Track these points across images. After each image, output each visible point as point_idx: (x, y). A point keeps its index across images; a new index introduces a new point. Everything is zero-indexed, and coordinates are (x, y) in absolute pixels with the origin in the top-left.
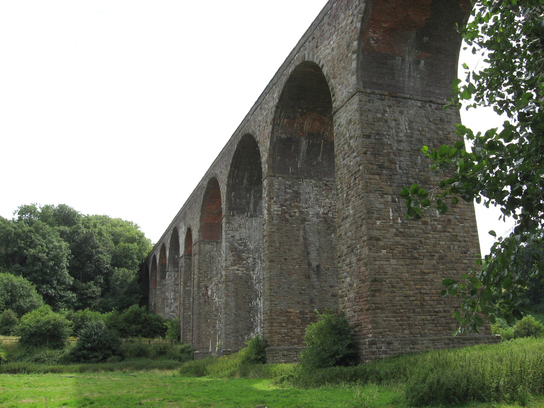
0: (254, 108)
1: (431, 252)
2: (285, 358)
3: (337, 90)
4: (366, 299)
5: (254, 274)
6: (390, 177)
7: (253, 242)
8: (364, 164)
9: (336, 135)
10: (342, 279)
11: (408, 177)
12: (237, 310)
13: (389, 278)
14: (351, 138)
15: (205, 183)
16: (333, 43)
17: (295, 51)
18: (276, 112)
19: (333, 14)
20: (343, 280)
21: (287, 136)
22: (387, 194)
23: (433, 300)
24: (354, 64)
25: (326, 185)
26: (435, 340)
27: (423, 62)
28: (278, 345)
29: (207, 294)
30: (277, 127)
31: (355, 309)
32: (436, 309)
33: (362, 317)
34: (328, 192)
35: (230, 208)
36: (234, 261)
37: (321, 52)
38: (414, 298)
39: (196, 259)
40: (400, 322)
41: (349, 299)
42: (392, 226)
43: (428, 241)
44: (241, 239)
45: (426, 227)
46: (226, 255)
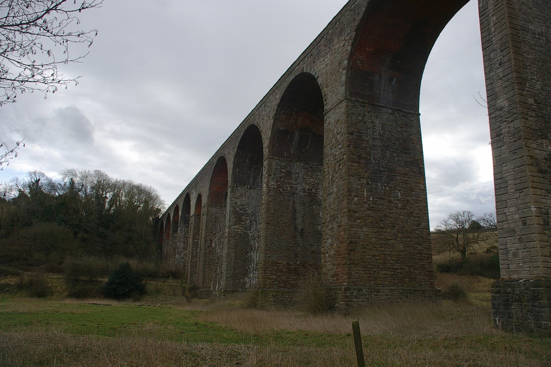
0: (259, 105)
1: (393, 224)
2: (274, 298)
3: (329, 96)
4: (344, 256)
5: (250, 232)
6: (366, 165)
8: (348, 154)
9: (326, 131)
10: (325, 240)
11: (379, 167)
12: (235, 260)
13: (362, 241)
14: (338, 134)
15: (215, 161)
16: (328, 60)
17: (296, 64)
18: (277, 110)
19: (328, 37)
20: (326, 241)
21: (284, 129)
22: (363, 178)
23: (393, 260)
24: (344, 78)
25: (312, 168)
26: (393, 290)
27: (395, 79)
28: (269, 288)
29: (211, 246)
30: (277, 121)
31: (334, 263)
32: (395, 267)
33: (340, 270)
34: (313, 173)
35: (235, 181)
36: (236, 221)
37: (317, 67)
38: (379, 258)
39: (204, 219)
40: (368, 275)
41: (329, 256)
42: (365, 202)
43: (392, 215)
44: (241, 206)
45: (390, 205)
46: (229, 217)
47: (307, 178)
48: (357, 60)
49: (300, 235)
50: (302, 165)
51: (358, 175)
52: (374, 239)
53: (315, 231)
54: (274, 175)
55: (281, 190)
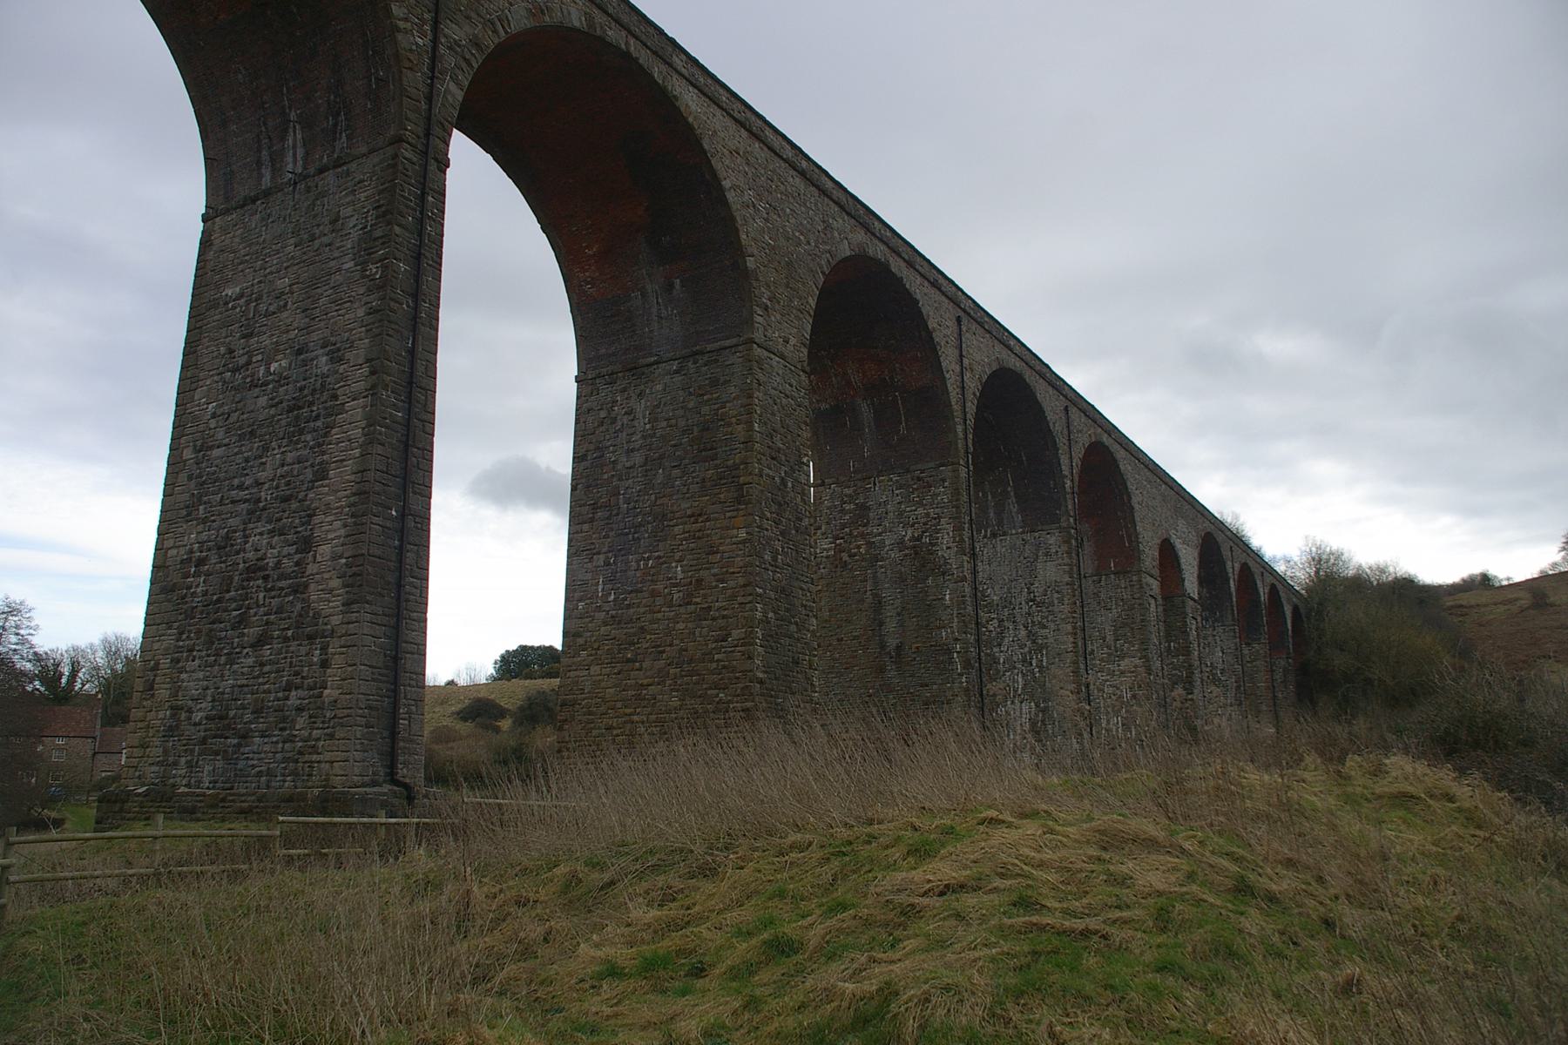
5: (1002, 652)
7: (999, 586)
21: (831, 406)
47: (908, 509)
48: (582, 286)
49: (896, 662)
50: (894, 479)
51: (587, 550)
52: (610, 690)
53: (931, 646)
54: (828, 523)
55: (845, 556)
